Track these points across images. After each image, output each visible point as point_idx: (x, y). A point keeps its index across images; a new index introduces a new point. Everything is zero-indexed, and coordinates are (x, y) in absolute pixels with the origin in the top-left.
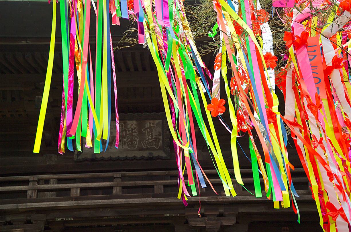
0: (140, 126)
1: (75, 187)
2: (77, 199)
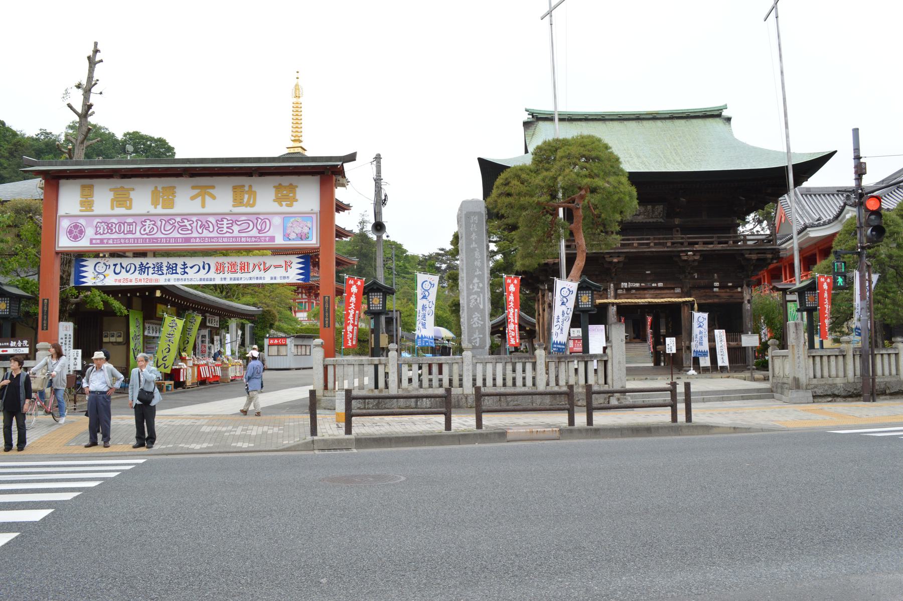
0: (653, 208)
1: (635, 243)
2: (636, 248)
